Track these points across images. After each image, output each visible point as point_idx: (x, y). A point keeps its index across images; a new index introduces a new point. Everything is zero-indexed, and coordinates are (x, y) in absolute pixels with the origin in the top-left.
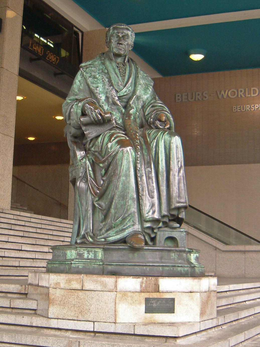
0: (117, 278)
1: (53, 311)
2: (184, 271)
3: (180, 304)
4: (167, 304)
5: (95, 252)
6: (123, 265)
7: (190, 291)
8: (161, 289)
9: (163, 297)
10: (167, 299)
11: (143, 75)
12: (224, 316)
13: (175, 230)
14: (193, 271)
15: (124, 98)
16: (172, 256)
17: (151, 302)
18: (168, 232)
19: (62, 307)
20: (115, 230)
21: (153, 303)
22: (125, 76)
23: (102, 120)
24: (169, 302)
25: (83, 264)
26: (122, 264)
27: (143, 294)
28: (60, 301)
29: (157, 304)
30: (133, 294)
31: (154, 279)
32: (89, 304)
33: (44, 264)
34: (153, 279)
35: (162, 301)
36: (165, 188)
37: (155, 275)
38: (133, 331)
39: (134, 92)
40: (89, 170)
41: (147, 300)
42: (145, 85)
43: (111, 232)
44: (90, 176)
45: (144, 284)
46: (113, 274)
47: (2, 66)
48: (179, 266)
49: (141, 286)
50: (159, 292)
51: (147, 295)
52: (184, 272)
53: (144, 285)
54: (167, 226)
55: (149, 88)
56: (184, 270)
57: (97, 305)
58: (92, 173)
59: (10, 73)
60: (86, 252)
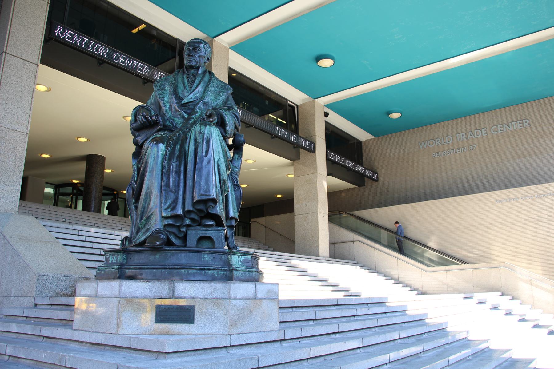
6: (141, 268)
13: (210, 229)
15: (191, 105)
16: (204, 258)
20: (143, 231)
23: (147, 122)
33: (94, 272)
39: (202, 98)
43: (140, 234)
51: (159, 302)
56: (218, 274)
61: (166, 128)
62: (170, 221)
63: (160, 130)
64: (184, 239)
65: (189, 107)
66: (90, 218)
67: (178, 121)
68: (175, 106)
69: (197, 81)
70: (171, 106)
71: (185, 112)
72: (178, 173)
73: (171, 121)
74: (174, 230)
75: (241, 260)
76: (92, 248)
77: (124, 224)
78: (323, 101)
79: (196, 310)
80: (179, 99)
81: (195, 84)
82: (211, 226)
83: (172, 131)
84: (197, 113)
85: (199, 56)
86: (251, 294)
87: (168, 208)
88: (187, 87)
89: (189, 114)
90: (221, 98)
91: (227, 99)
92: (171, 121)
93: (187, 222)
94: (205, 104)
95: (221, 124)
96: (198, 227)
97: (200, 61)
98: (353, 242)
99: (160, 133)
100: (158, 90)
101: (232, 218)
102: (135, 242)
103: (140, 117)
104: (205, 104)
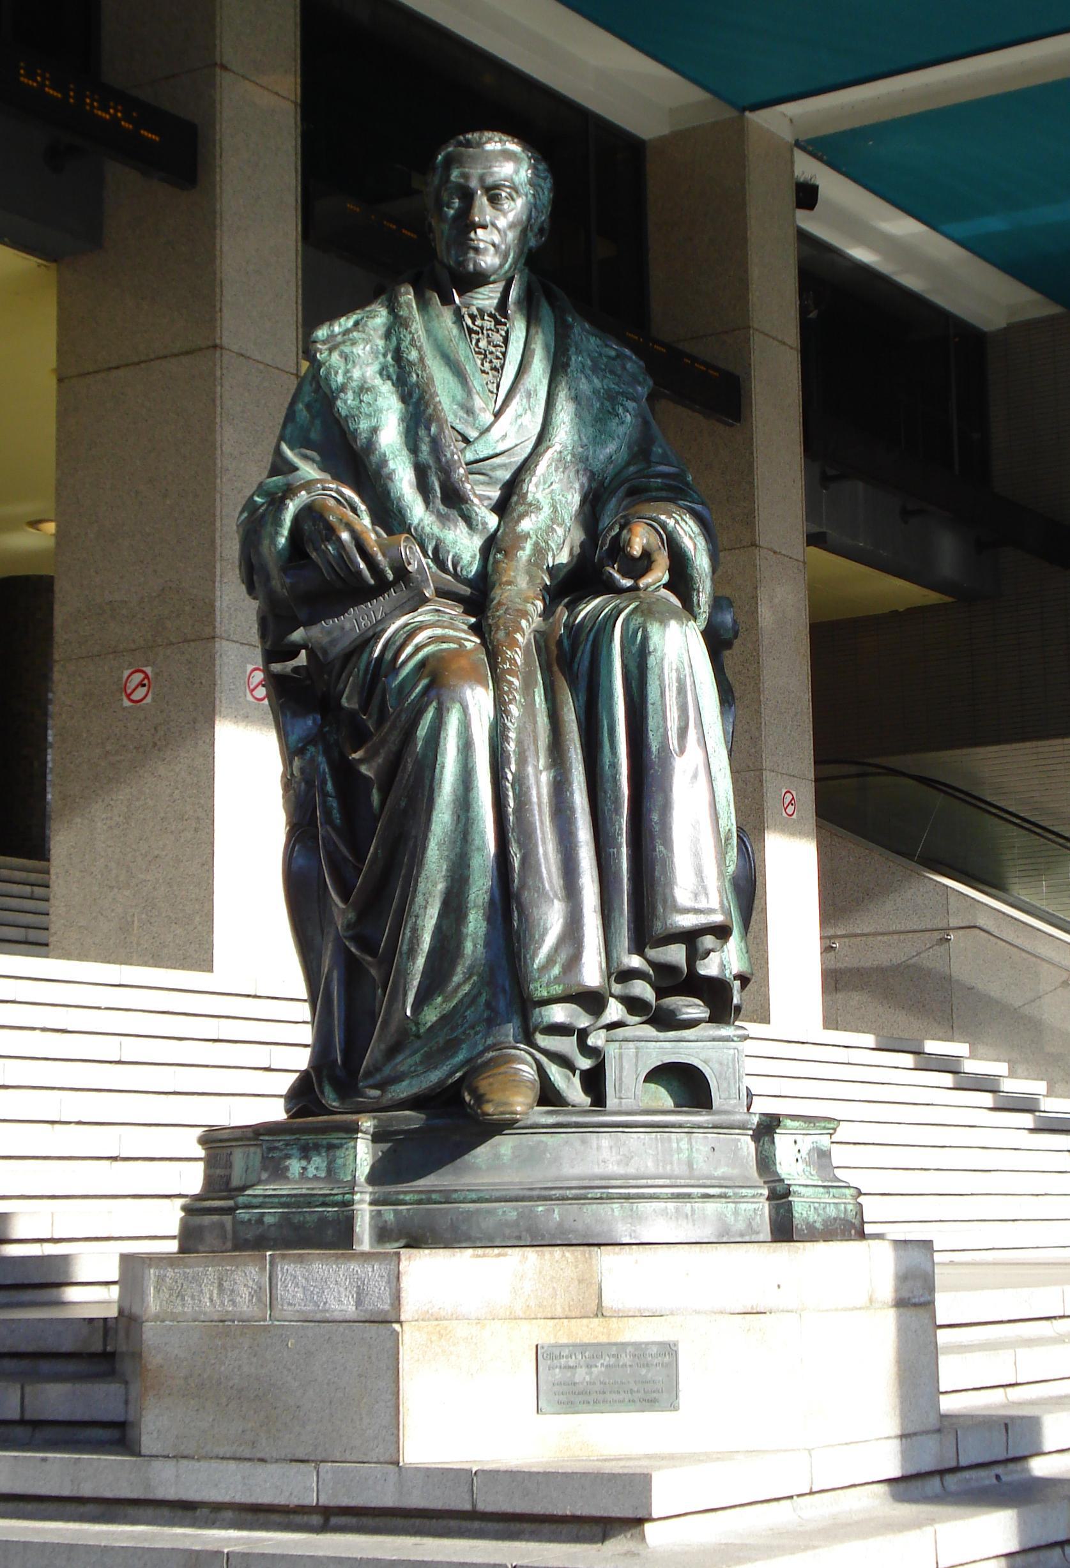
1: (156, 1426)
4: (644, 1371)
10: (639, 1350)
11: (600, 354)
15: (503, 466)
19: (192, 1402)
22: (498, 370)
25: (283, 1205)
28: (186, 1378)
32: (296, 1384)
35: (616, 1356)
37: (591, 1241)
38: (467, 1497)
40: (325, 794)
42: (599, 399)
44: (328, 819)
47: (218, 341)
51: (547, 1334)
52: (736, 1220)
55: (621, 410)
56: (736, 1213)
57: (328, 1384)
58: (335, 805)
59: (261, 367)
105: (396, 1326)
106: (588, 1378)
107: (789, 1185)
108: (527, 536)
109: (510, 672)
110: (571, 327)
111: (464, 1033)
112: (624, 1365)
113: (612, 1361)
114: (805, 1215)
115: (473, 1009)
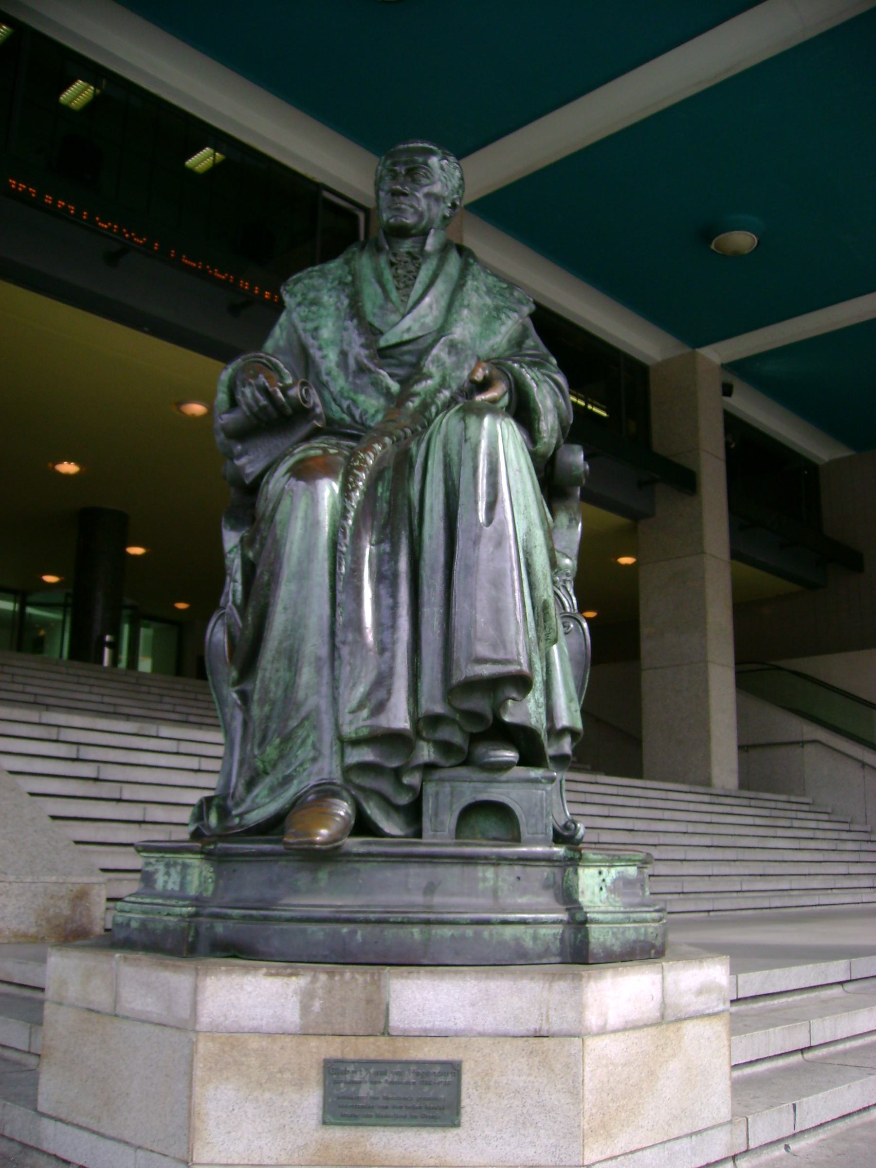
0: (197, 974)
2: (539, 942)
3: (488, 1088)
4: (426, 1089)
5: (185, 866)
7: (532, 1033)
8: (397, 1019)
9: (405, 1057)
12: (794, 1106)
14: (581, 941)
15: (409, 352)
16: (485, 879)
17: (348, 1077)
18: (472, 784)
20: (268, 781)
21: (359, 1083)
23: (271, 409)
24: (432, 1078)
25: (144, 912)
26: (261, 915)
27: (313, 1042)
29: (380, 1087)
30: (270, 1040)
31: (365, 981)
34: (360, 979)
35: (399, 1074)
36: (436, 609)
39: (442, 330)
41: (333, 1071)
43: (261, 790)
45: (320, 999)
46: (230, 954)
48: (505, 922)
49: (305, 1009)
50: (389, 1035)
51: (333, 1049)
53: (317, 1005)
54: (467, 761)
56: (535, 938)
60: (161, 868)
61: (333, 429)
62: (367, 755)
63: (316, 433)
64: (413, 814)
65: (407, 360)
66: (92, 681)
67: (371, 404)
68: (357, 350)
69: (424, 276)
70: (343, 354)
71: (391, 375)
72: (385, 578)
73: (345, 404)
74: (385, 786)
75: (609, 881)
76: (96, 780)
77: (179, 694)
78: (716, 354)
79: (467, 1079)
80: (371, 332)
81: (418, 288)
82: (506, 766)
83: (356, 438)
84: (430, 376)
85: (428, 196)
86: (650, 1009)
87: (361, 706)
88: (394, 295)
89: (406, 382)
90: (504, 329)
91: (523, 335)
92: (345, 404)
93: (426, 753)
94: (453, 347)
95: (523, 412)
96: (463, 771)
97: (429, 209)
98: (802, 743)
99: (315, 443)
100: (299, 304)
101: (565, 731)
102: (240, 815)
103: (248, 391)
104: (453, 347)
105: (192, 1035)
106: (372, 1093)
107: (586, 913)
108: (417, 394)
109: (360, 469)
110: (471, 265)
111: (295, 770)
112: (408, 1083)
113: (396, 1078)
114: (602, 939)
115: (302, 749)
